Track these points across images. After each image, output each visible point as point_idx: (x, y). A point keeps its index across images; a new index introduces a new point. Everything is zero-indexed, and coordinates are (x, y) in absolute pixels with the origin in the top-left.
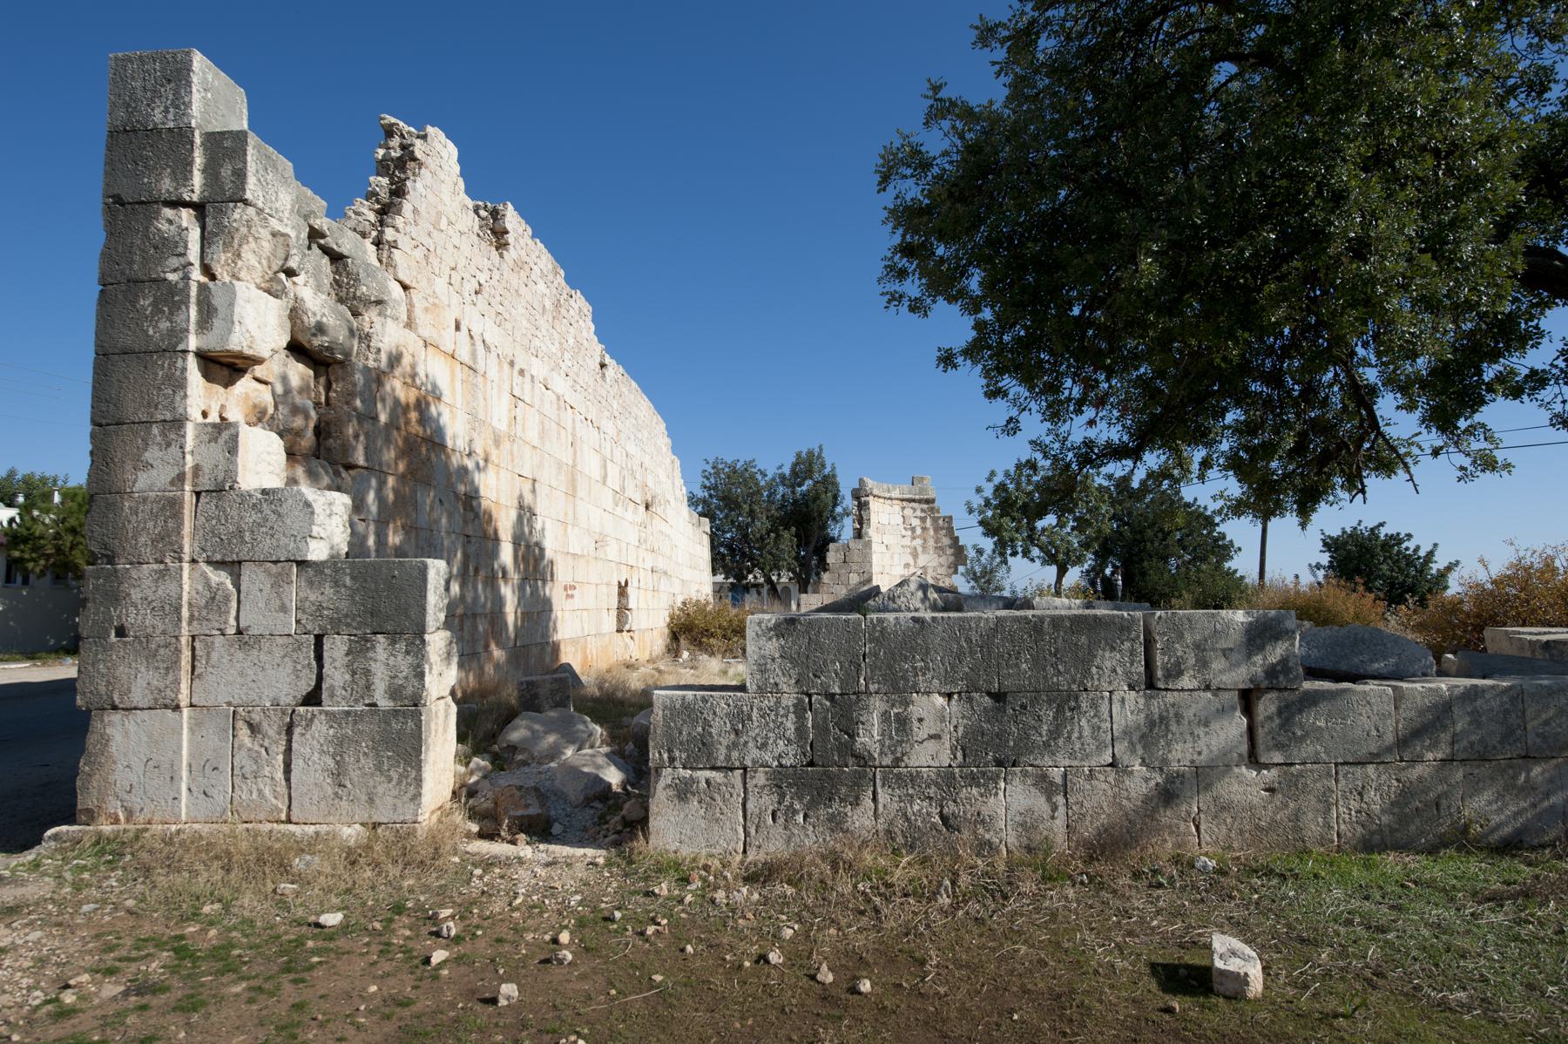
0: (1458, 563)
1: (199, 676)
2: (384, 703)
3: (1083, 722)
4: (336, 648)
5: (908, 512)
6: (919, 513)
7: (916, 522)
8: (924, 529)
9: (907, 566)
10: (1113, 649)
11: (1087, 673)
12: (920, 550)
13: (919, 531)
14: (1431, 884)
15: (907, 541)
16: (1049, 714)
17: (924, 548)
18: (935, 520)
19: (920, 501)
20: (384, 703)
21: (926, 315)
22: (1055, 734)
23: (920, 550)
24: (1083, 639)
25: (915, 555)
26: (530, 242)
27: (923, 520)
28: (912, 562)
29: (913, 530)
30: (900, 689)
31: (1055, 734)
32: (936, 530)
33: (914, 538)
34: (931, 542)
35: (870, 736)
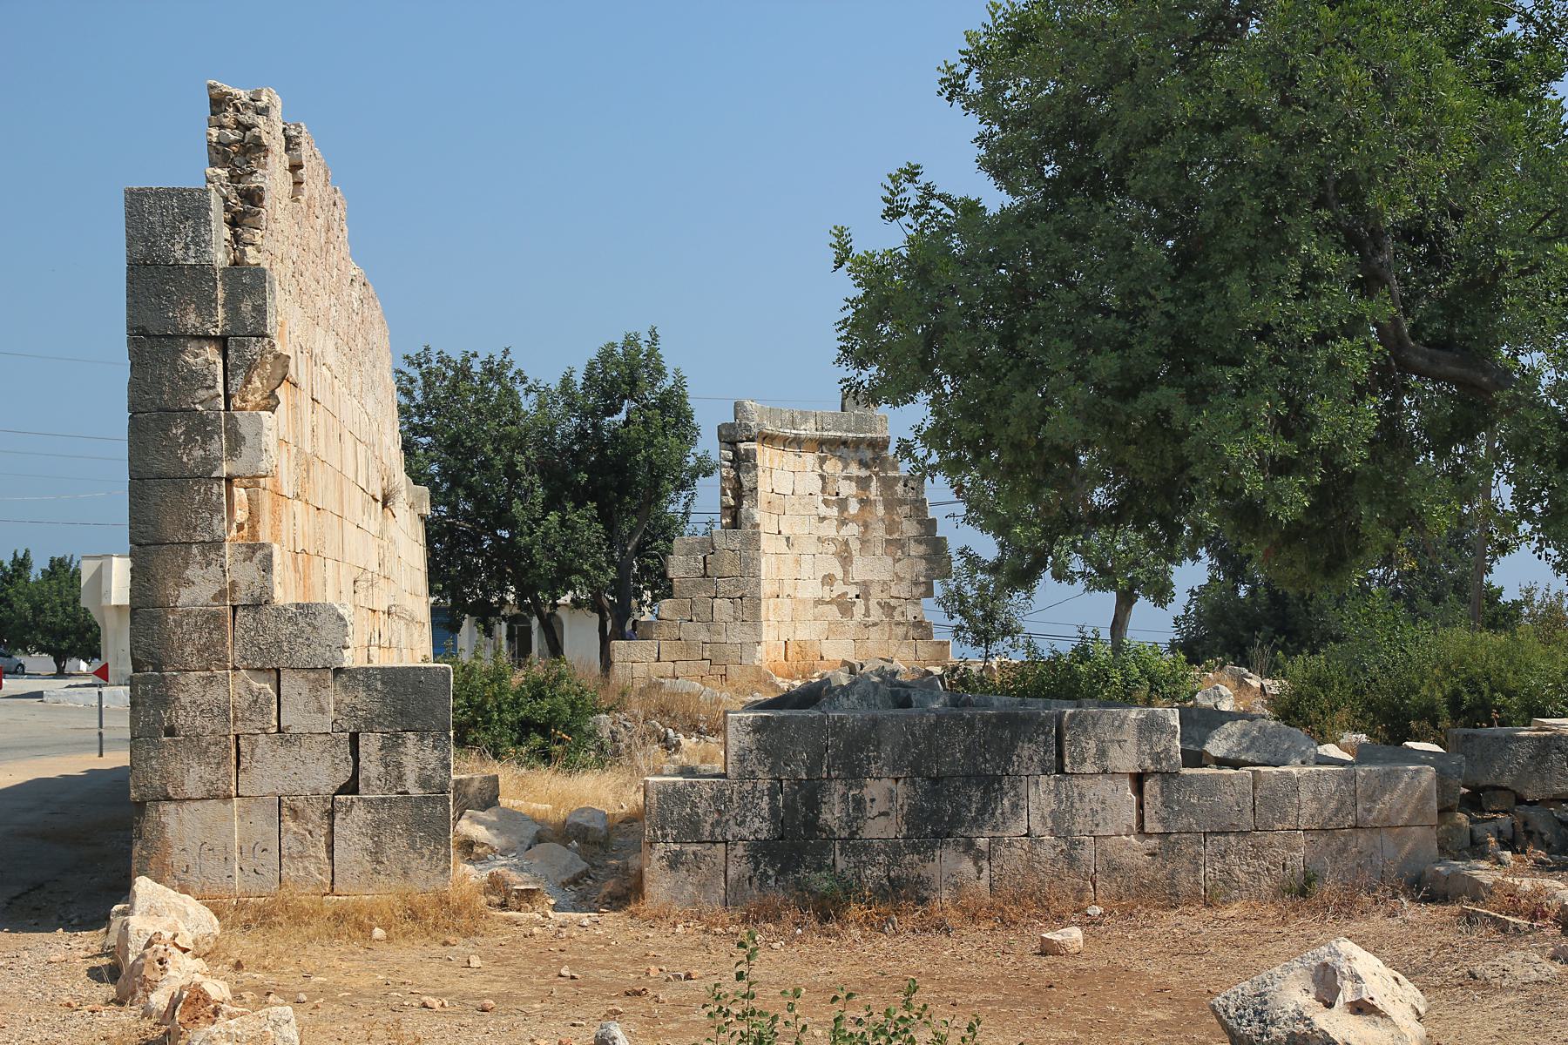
2: (416, 791)
3: (1005, 801)
4: (371, 744)
7: (848, 489)
8: (864, 503)
9: (828, 580)
10: (1030, 741)
11: (1009, 761)
12: (855, 546)
13: (854, 508)
15: (829, 529)
16: (976, 795)
20: (416, 791)
22: (982, 810)
23: (855, 546)
24: (1007, 734)
25: (845, 559)
27: (863, 483)
28: (839, 574)
29: (842, 504)
30: (855, 774)
31: (982, 810)
32: (890, 505)
33: (843, 522)
34: (879, 532)
35: (832, 814)
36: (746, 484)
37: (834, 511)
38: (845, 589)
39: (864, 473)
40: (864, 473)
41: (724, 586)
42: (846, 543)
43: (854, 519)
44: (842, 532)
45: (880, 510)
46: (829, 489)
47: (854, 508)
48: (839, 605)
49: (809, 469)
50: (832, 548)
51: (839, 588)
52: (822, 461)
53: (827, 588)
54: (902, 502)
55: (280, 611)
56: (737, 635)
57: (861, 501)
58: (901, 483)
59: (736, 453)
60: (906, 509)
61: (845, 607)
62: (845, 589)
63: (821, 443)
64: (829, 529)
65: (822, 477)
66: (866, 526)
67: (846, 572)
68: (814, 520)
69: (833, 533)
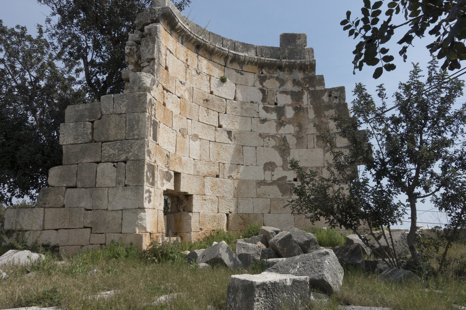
6: (289, 86)
7: (284, 100)
8: (298, 110)
9: (269, 166)
12: (292, 141)
13: (290, 113)
17: (299, 137)
25: (283, 148)
27: (297, 97)
28: (278, 161)
29: (280, 111)
32: (318, 111)
33: (281, 124)
34: (311, 130)
37: (274, 116)
38: (285, 173)
39: (296, 89)
40: (296, 89)
41: (108, 150)
42: (284, 139)
43: (290, 122)
44: (280, 132)
45: (311, 115)
46: (269, 99)
47: (290, 113)
48: (280, 186)
49: (251, 83)
50: (273, 143)
52: (262, 79)
53: (268, 173)
54: (329, 107)
55: (200, 270)
56: (119, 200)
57: (296, 109)
58: (326, 94)
60: (332, 112)
62: (285, 173)
63: (261, 65)
66: (300, 126)
68: (255, 121)
69: (273, 131)
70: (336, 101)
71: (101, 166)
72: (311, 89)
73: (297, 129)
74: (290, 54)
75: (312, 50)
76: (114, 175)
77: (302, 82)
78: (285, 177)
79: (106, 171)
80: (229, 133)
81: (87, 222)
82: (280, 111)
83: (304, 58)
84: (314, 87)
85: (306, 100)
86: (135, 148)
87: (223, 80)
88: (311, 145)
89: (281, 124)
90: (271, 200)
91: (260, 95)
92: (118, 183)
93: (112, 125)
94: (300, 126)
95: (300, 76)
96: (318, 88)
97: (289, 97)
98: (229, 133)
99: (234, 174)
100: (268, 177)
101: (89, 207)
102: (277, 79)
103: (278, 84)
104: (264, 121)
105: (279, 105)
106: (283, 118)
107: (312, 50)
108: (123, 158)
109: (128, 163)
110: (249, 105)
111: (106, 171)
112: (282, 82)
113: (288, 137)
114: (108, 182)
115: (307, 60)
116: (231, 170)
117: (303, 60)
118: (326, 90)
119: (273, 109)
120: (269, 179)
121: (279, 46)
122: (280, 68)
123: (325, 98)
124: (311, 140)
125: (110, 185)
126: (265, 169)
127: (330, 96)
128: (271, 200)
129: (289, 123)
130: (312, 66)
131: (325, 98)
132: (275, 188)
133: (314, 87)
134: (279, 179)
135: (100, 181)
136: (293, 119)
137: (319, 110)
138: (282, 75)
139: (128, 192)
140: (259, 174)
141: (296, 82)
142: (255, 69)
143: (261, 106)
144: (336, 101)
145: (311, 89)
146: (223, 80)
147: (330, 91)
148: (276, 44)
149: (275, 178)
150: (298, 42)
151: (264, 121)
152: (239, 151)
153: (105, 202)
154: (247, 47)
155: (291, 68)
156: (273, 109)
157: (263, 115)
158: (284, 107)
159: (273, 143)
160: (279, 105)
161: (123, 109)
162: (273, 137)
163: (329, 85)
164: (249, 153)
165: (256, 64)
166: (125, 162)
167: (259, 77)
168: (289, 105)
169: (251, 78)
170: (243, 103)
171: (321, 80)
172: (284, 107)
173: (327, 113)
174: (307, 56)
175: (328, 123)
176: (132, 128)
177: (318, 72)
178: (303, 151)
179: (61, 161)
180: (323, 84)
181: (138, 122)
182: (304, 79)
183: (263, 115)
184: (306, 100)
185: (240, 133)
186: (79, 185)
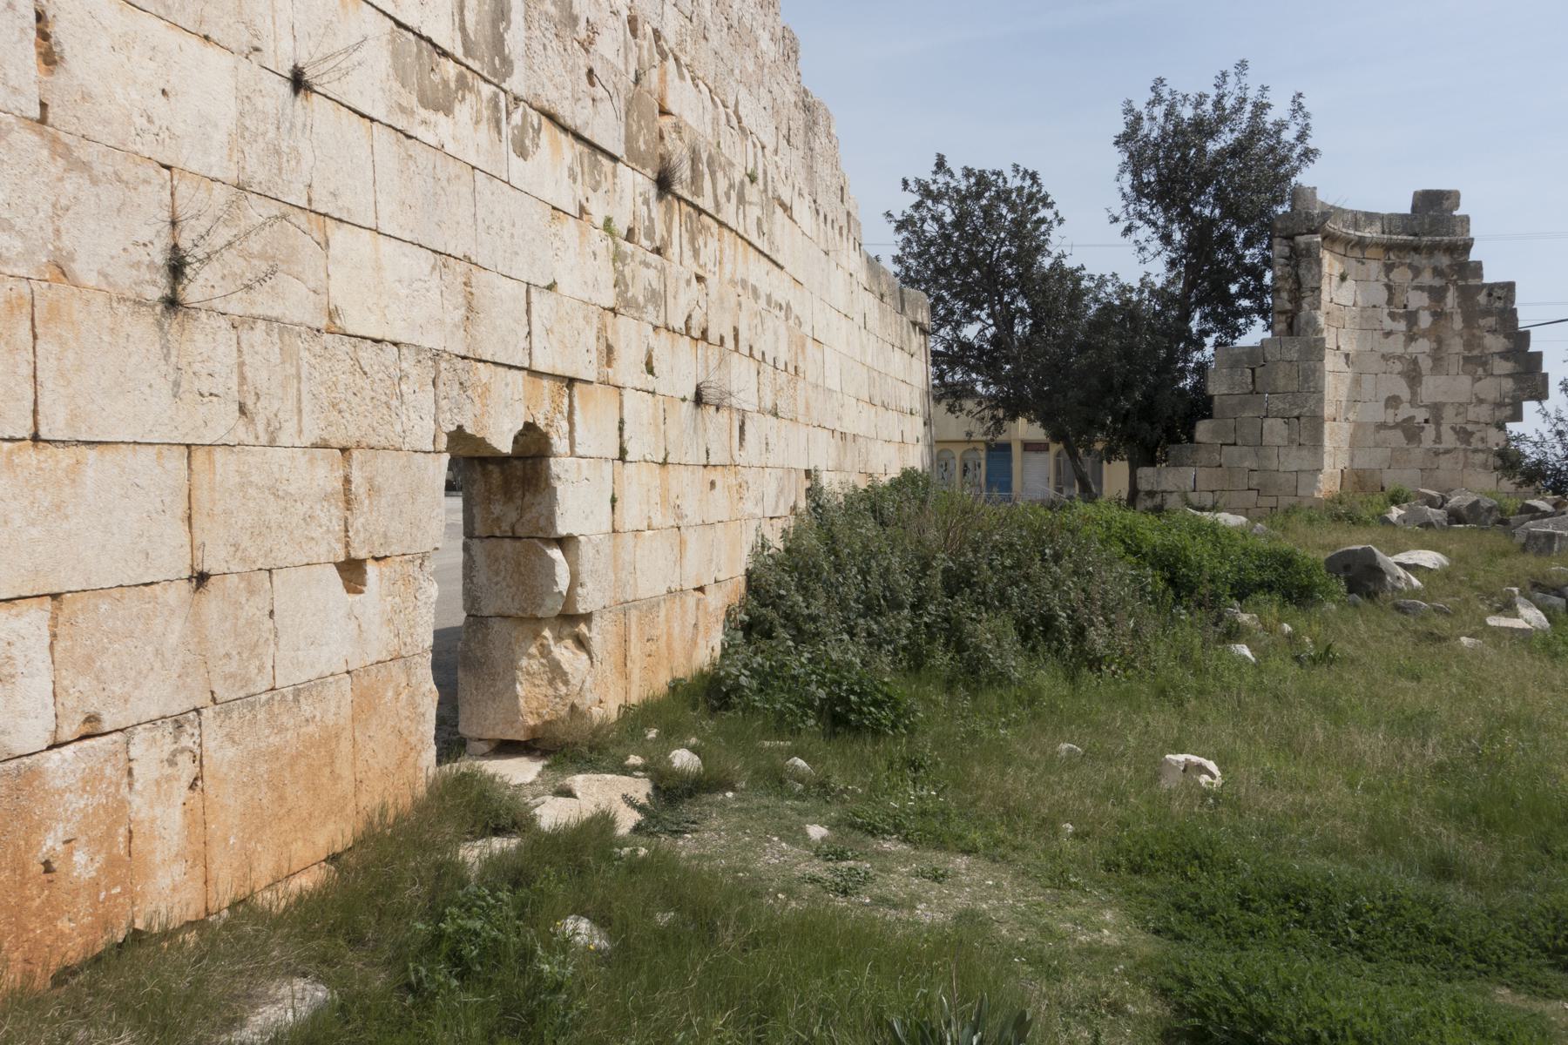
0: (624, 797)
1: (92, 719)
5: (1401, 276)
6: (1427, 278)
7: (1418, 300)
8: (1438, 315)
9: (1393, 402)
12: (1426, 364)
13: (1425, 320)
14: (895, 906)
15: (1396, 345)
17: (1437, 358)
18: (1467, 294)
19: (1432, 249)
21: (1117, 143)
23: (1426, 364)
25: (1413, 376)
26: (459, 420)
27: (1437, 294)
28: (1405, 393)
29: (1411, 317)
32: (1469, 320)
33: (1411, 338)
34: (1456, 345)
36: (1308, 282)
37: (1401, 326)
39: (1438, 282)
40: (1438, 282)
42: (1415, 362)
44: (1410, 350)
45: (1458, 323)
46: (1396, 300)
47: (1425, 320)
48: (1405, 431)
49: (1373, 278)
50: (1398, 367)
51: (1405, 411)
52: (1389, 268)
53: (1391, 411)
54: (1487, 313)
56: (1293, 460)
58: (1485, 292)
59: (1292, 249)
60: (1491, 321)
61: (1411, 431)
63: (1388, 247)
64: (1396, 345)
65: (1389, 287)
66: (1440, 341)
67: (1414, 394)
68: (1378, 335)
69: (1400, 350)
70: (1499, 304)
71: (1268, 422)
72: (1461, 283)
73: (1434, 345)
74: (1431, 225)
75: (1466, 220)
76: (1286, 433)
77: (1447, 271)
78: (1413, 418)
79: (1275, 430)
80: (1347, 356)
81: (1254, 483)
82: (1411, 317)
83: (1454, 233)
84: (1465, 279)
85: (1451, 299)
86: (1312, 402)
87: (1343, 278)
88: (1453, 370)
89: (1411, 338)
90: (1393, 450)
91: (1385, 294)
92: (1291, 441)
93: (1281, 375)
94: (1440, 341)
95: (1444, 261)
96: (1472, 282)
97: (1425, 295)
98: (1347, 356)
99: (1351, 416)
100: (1390, 417)
101: (1254, 466)
102: (1410, 266)
103: (1410, 275)
104: (1388, 334)
105: (1410, 308)
106: (1415, 329)
107: (1466, 220)
108: (1296, 413)
109: (1303, 420)
110: (1370, 312)
111: (1275, 430)
112: (1417, 272)
113: (1421, 358)
114: (1278, 441)
115: (1458, 238)
116: (1348, 409)
117: (1454, 238)
118: (1485, 285)
119: (1401, 316)
120: (1390, 421)
121: (1408, 211)
122: (1416, 249)
123: (1482, 298)
124: (1454, 364)
125: (1282, 443)
126: (1386, 407)
127: (1490, 295)
128: (1393, 450)
129: (1423, 336)
130: (1467, 246)
131: (1482, 298)
132: (1399, 433)
133: (1465, 279)
134: (1405, 421)
135: (1267, 439)
136: (1429, 330)
137: (1471, 316)
138: (1417, 259)
139: (1305, 453)
140: (1378, 413)
141: (1437, 272)
142: (1379, 252)
143: (1386, 311)
144: (1499, 304)
145: (1461, 283)
146: (1343, 278)
147: (1491, 288)
148: (1406, 209)
149: (1399, 419)
150: (1446, 204)
151: (1388, 334)
152: (1357, 382)
153: (1276, 462)
154: (1370, 217)
155: (1432, 249)
156: (1401, 316)
157: (1388, 324)
158: (1416, 312)
159: (1398, 367)
160: (1410, 308)
161: (1295, 356)
162: (1400, 358)
163: (1489, 277)
164: (1368, 381)
165: (1383, 245)
166: (1298, 418)
167: (1385, 265)
168: (1425, 308)
169: (1374, 267)
170: (1363, 309)
171: (1478, 268)
172: (1416, 312)
173: (1482, 322)
174: (1458, 230)
175: (1481, 338)
176: (1306, 380)
177: (1473, 256)
178: (1441, 380)
179: (1210, 410)
180: (1481, 277)
181: (1314, 371)
182: (1450, 266)
183: (1388, 324)
184: (1451, 299)
185: (1359, 354)
186: (1239, 442)
